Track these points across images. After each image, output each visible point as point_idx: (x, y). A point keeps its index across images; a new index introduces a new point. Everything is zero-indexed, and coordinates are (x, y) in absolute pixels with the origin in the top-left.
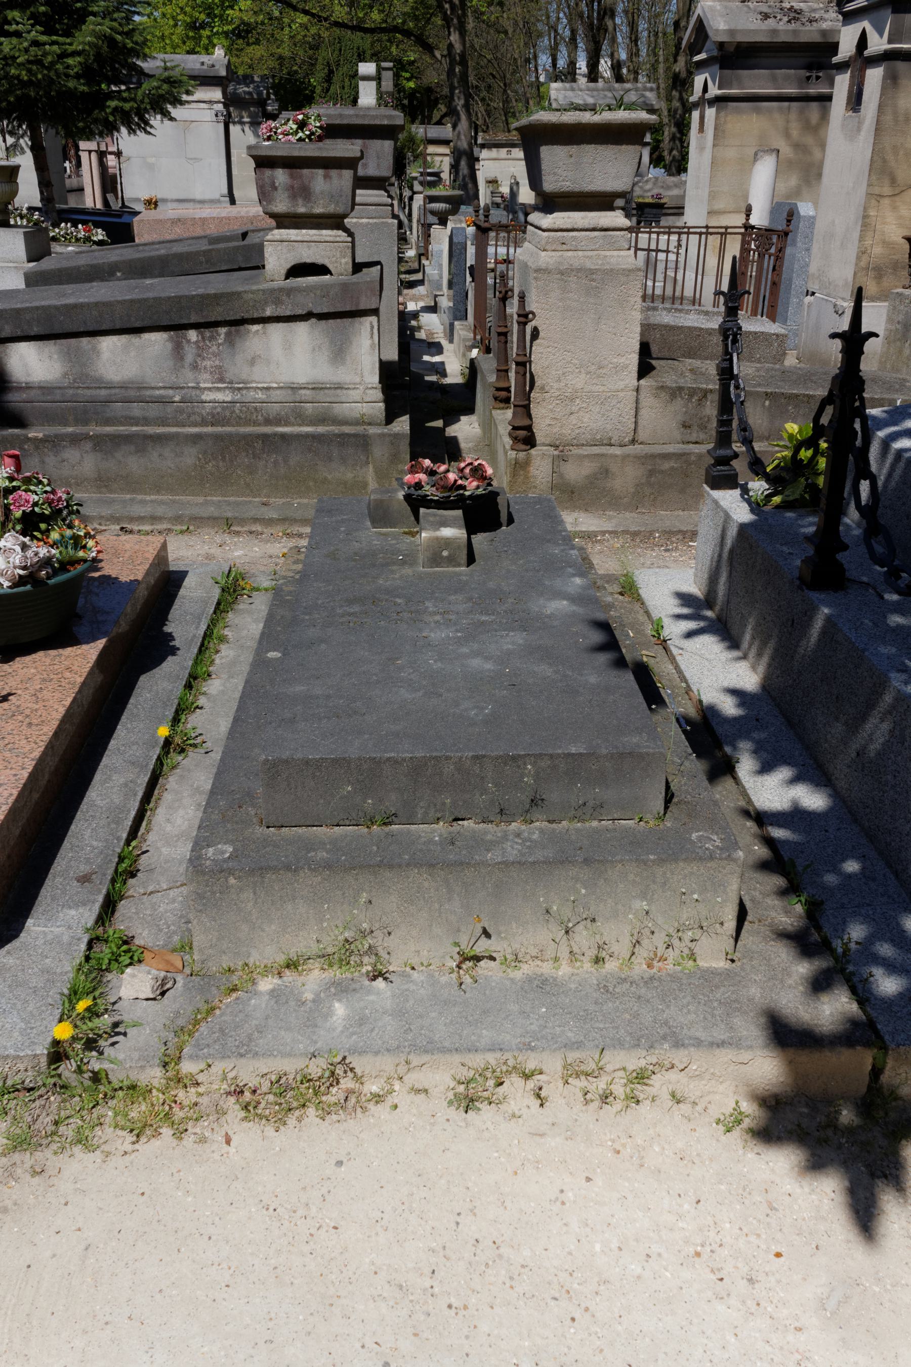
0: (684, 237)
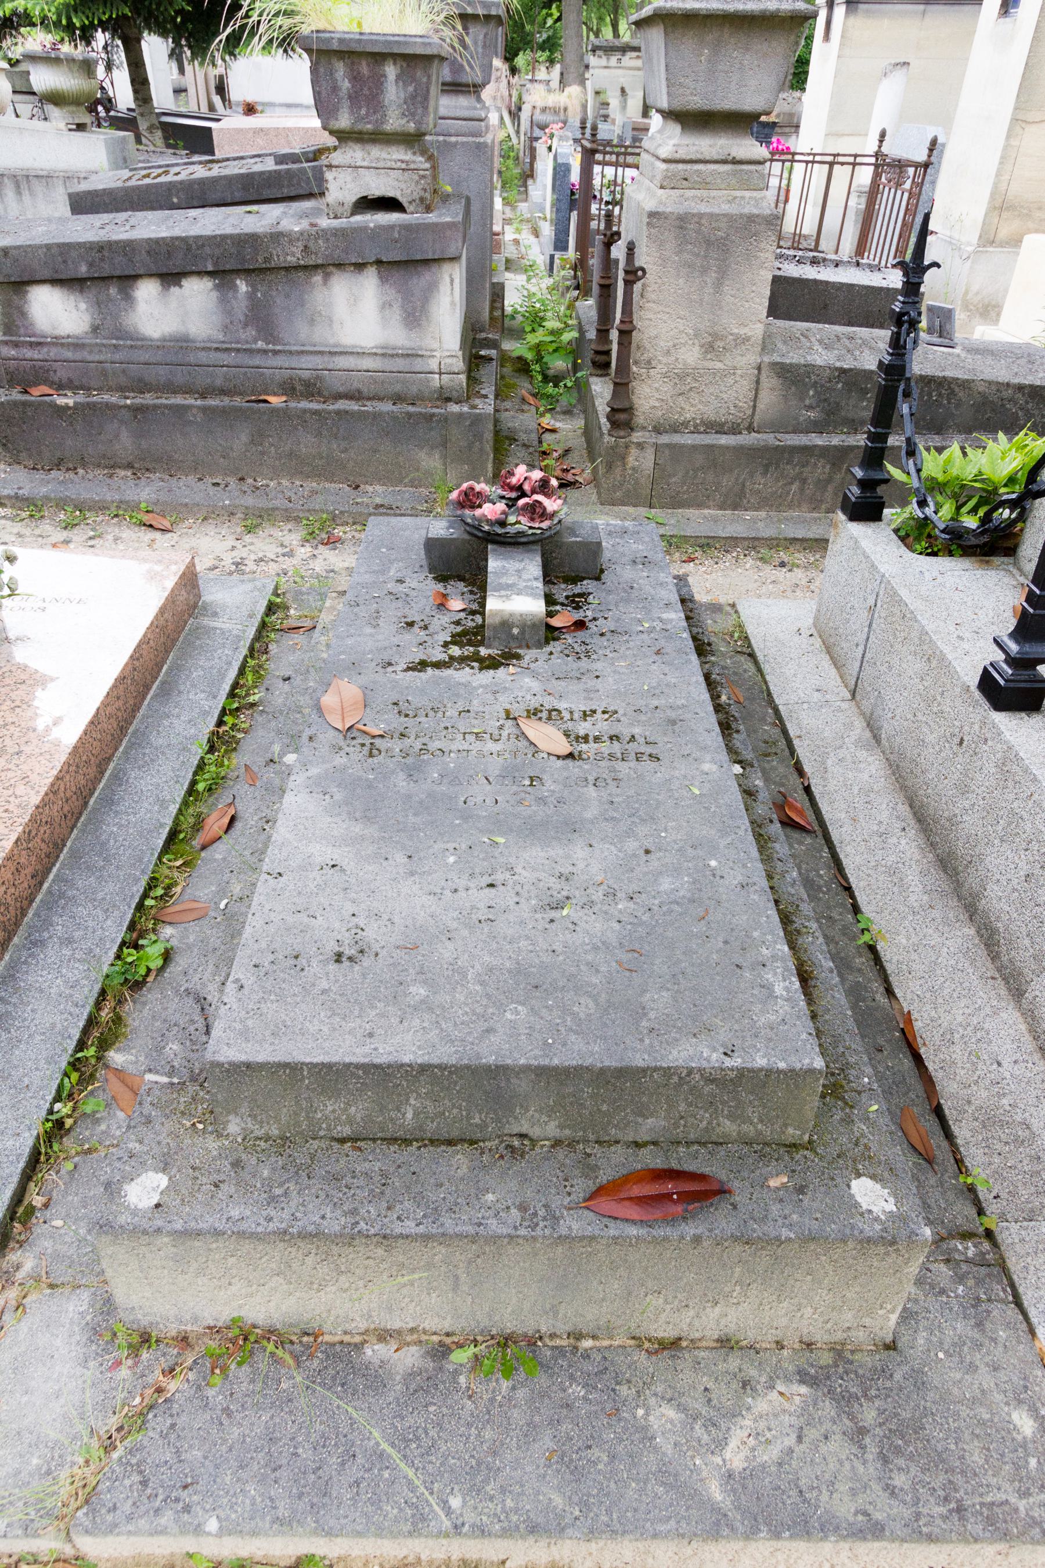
0: (788, 164)
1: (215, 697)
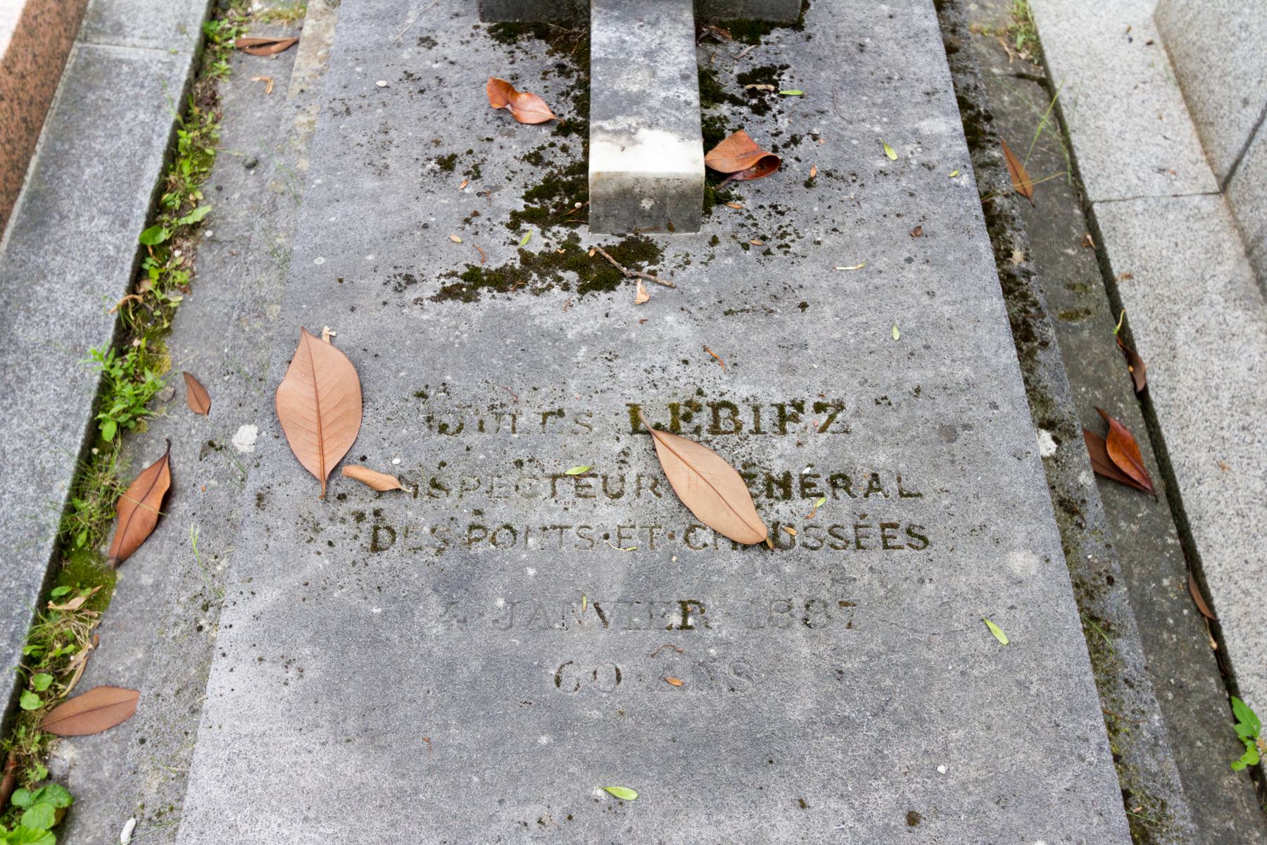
1: (124, 224)
